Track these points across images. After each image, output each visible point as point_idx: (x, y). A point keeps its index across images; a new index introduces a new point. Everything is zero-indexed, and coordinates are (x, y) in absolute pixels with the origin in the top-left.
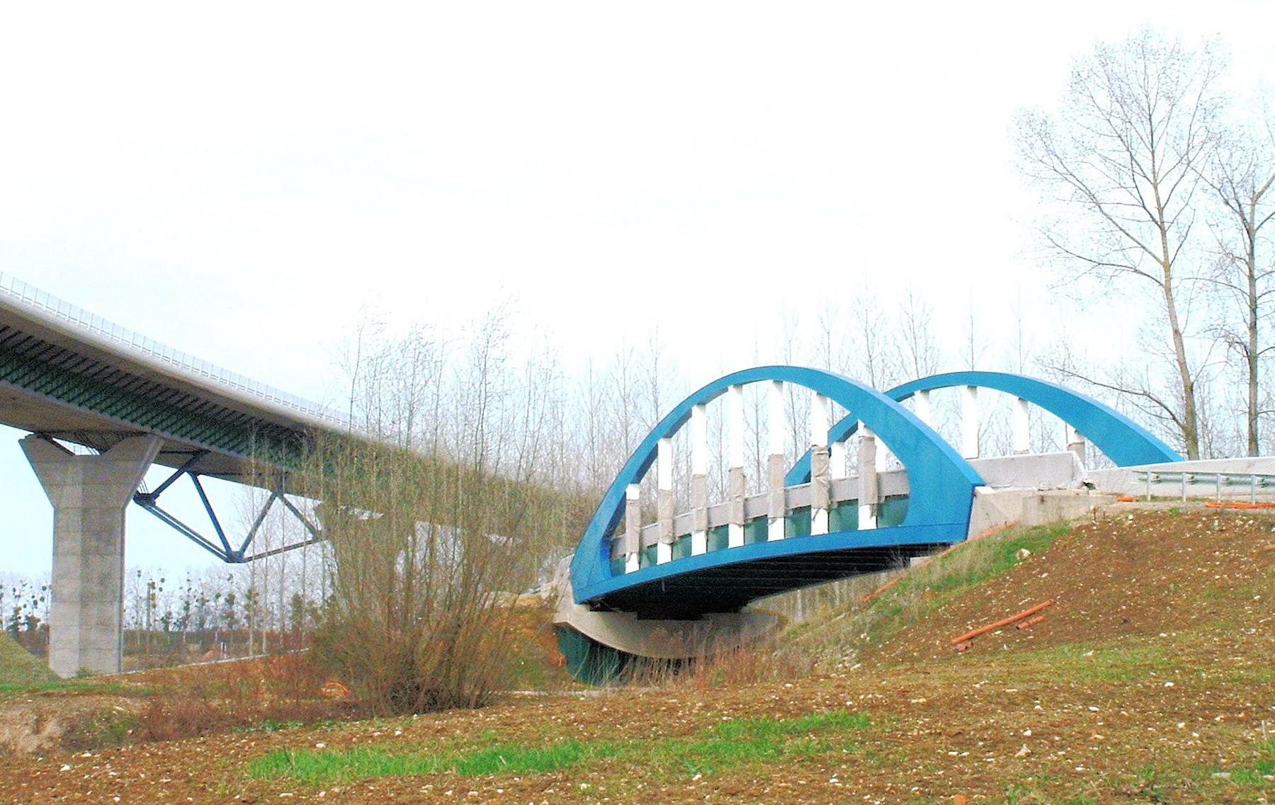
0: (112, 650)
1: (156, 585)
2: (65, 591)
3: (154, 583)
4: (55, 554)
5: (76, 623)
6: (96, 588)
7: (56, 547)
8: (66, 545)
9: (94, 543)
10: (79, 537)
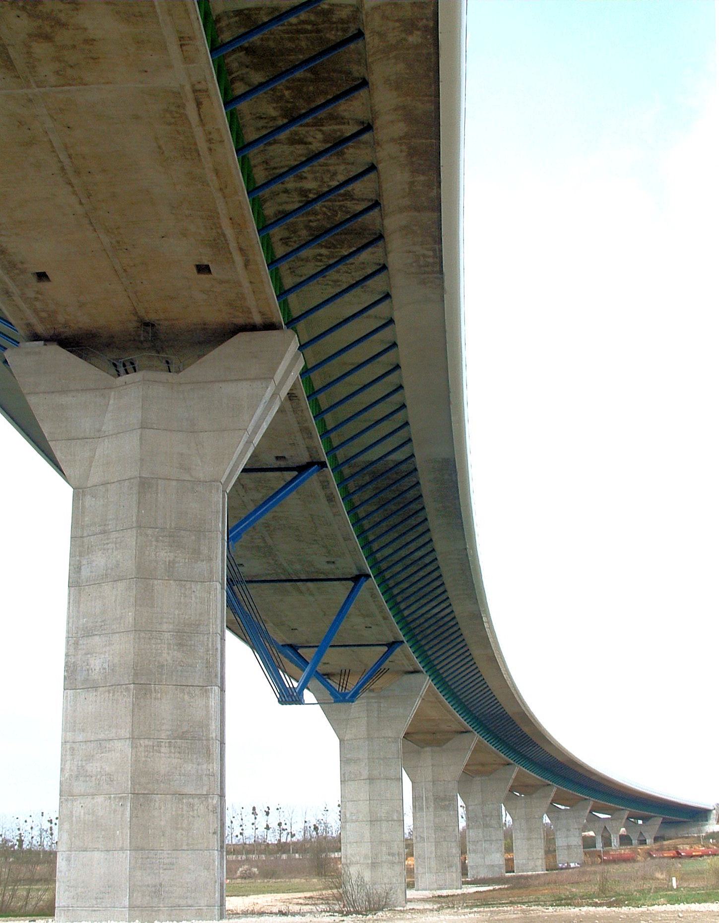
0: (206, 796)
1: (53, 821)
2: (96, 663)
3: (51, 820)
4: (76, 583)
5: (125, 732)
6: (168, 656)
7: (75, 569)
8: (100, 560)
9: (165, 555)
10: (131, 538)
